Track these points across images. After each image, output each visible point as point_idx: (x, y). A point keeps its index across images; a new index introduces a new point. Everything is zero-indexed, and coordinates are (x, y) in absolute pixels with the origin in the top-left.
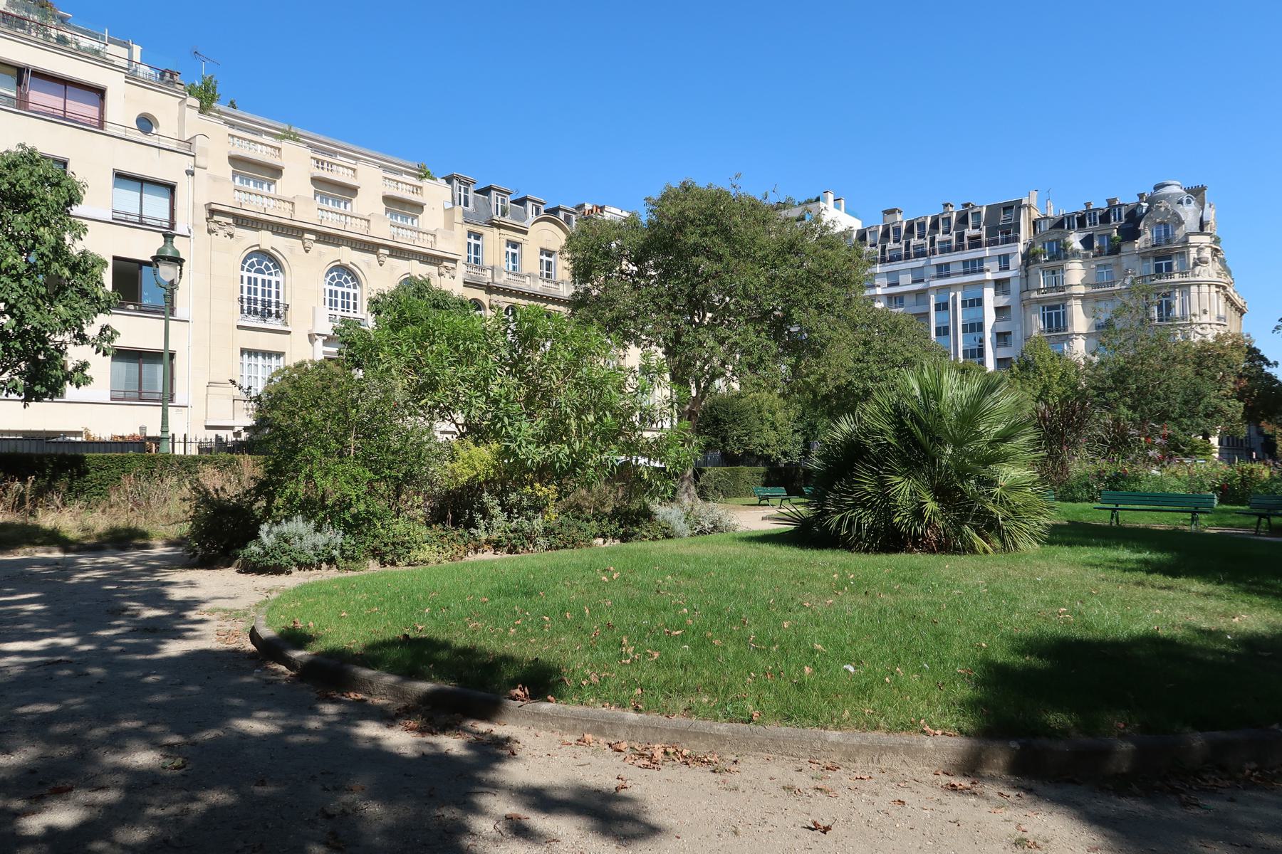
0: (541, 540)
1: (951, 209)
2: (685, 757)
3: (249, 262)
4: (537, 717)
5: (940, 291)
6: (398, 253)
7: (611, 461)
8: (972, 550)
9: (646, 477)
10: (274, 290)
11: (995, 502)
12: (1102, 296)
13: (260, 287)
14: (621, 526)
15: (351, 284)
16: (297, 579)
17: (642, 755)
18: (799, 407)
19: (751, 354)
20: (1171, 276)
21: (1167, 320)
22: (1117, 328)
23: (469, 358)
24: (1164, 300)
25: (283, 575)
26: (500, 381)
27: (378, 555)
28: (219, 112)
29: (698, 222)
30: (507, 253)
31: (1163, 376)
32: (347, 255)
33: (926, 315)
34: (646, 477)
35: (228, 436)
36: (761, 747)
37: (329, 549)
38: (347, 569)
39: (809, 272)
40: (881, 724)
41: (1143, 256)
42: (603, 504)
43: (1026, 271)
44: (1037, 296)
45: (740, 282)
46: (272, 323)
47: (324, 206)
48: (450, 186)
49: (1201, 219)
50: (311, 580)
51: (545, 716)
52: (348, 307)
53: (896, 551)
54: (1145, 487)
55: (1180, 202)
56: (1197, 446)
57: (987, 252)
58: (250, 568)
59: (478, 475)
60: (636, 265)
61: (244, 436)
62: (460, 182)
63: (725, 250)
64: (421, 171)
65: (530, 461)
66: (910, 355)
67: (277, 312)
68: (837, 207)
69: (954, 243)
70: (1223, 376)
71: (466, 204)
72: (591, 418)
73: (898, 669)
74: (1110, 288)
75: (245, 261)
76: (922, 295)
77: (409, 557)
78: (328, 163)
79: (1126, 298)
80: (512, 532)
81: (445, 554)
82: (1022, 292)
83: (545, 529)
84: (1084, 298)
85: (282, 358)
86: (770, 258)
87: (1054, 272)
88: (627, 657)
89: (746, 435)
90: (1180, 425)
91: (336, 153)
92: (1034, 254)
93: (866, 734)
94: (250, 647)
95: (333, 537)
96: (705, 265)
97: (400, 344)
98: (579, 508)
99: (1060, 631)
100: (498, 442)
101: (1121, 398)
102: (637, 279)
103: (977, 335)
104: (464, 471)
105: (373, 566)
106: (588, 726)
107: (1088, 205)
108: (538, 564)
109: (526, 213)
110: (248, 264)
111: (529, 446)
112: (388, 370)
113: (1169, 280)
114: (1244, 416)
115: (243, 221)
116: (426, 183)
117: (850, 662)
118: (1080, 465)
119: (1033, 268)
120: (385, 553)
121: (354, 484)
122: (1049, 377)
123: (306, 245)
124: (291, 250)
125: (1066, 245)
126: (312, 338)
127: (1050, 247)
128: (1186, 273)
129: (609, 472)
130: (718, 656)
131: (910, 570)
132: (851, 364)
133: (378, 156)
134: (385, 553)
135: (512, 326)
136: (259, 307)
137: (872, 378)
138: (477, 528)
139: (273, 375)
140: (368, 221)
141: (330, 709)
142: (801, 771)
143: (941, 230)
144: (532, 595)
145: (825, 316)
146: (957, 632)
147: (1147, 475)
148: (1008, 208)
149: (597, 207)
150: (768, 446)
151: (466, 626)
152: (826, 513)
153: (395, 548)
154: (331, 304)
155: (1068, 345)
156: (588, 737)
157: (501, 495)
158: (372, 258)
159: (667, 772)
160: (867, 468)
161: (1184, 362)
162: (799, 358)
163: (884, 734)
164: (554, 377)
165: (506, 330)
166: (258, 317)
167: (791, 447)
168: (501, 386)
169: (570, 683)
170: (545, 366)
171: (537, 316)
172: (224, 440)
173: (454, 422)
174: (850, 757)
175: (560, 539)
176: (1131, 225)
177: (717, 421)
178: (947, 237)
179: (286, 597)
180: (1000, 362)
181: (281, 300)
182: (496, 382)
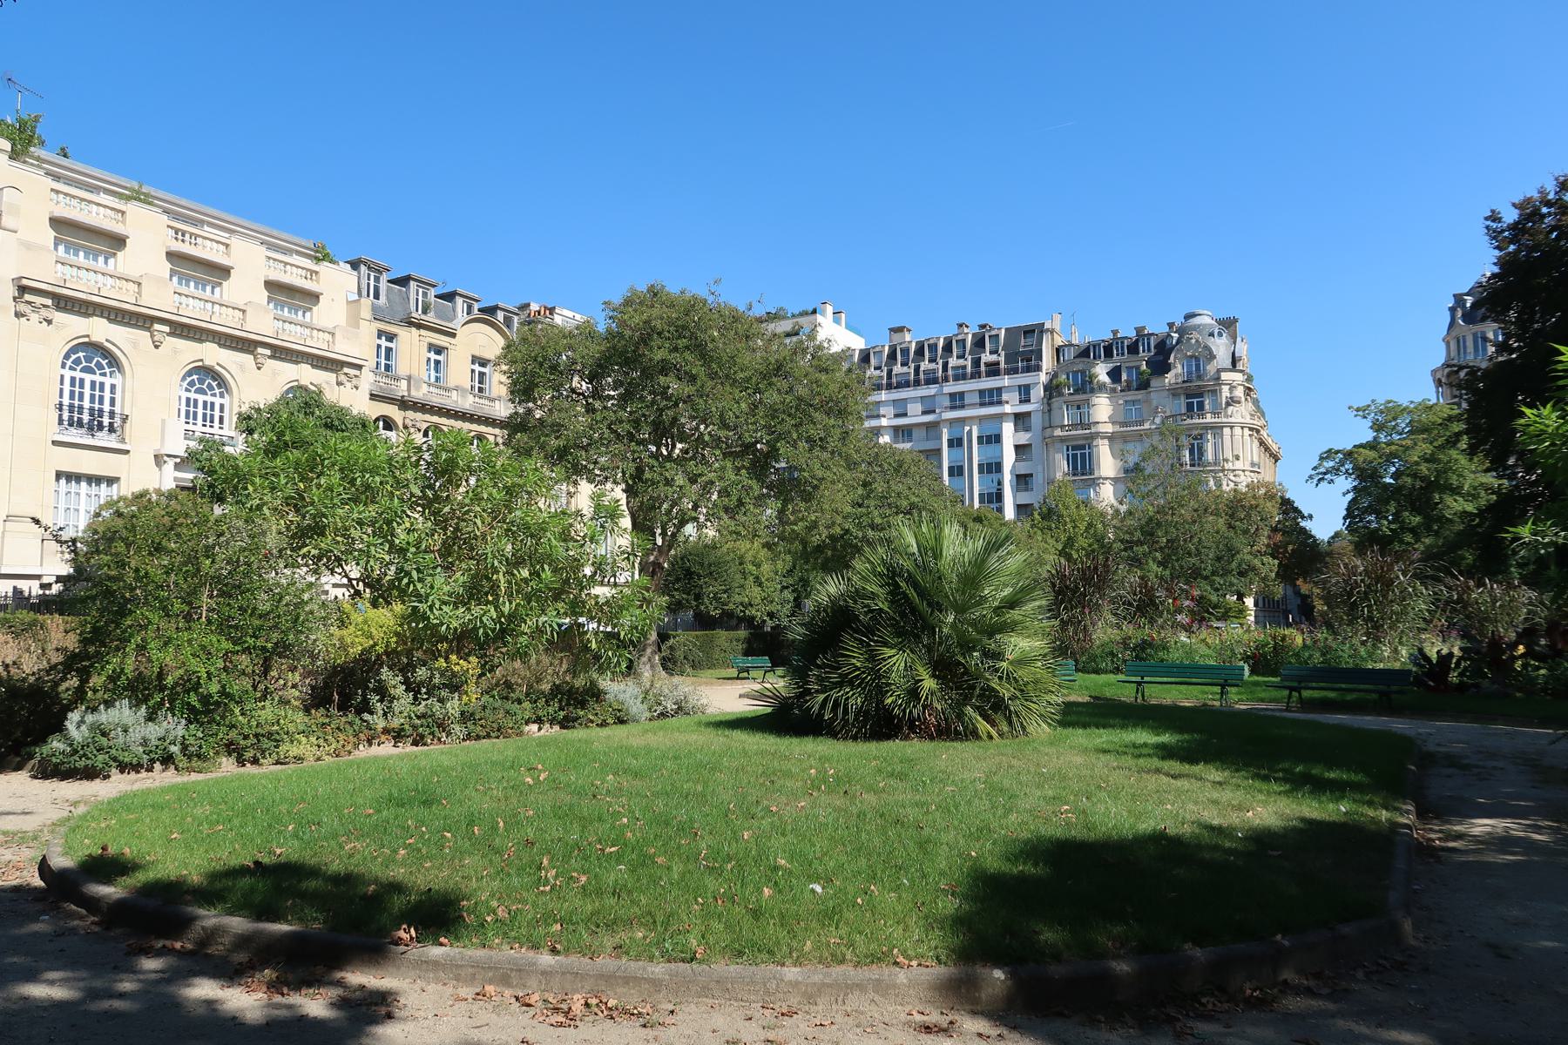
0: (457, 728)
1: (966, 330)
2: (611, 1009)
3: (74, 357)
4: (425, 965)
5: (953, 425)
6: (282, 353)
7: (550, 626)
8: (974, 734)
9: (594, 646)
10: (107, 395)
11: (1000, 678)
12: (1130, 436)
13: (87, 391)
14: (561, 709)
15: (217, 391)
16: (117, 785)
17: (556, 1010)
18: (788, 558)
19: (728, 495)
20: (1203, 416)
21: (1199, 465)
22: (1146, 473)
23: (366, 494)
24: (1196, 442)
25: (98, 781)
26: (408, 525)
27: (234, 751)
28: (38, 159)
29: (667, 335)
30: (429, 359)
31: (1196, 527)
32: (212, 354)
33: (938, 451)
34: (594, 646)
35: (32, 588)
36: (705, 991)
37: (166, 744)
38: (190, 770)
39: (798, 399)
40: (848, 957)
41: (1174, 392)
42: (539, 681)
43: (1049, 405)
44: (1061, 434)
45: (717, 408)
46: (103, 439)
47: (183, 289)
48: (355, 273)
49: (1233, 354)
50: (136, 787)
51: (435, 965)
52: (212, 421)
53: (888, 737)
54: (1175, 656)
55: (1212, 335)
56: (1230, 608)
57: (1006, 381)
58: (50, 771)
59: (375, 644)
60: (591, 383)
61: (56, 589)
62: (369, 268)
63: (698, 369)
64: (317, 252)
66: (916, 500)
67: (111, 425)
68: (837, 321)
69: (969, 369)
70: (1257, 529)
71: (377, 296)
72: (525, 573)
73: (872, 887)
74: (1139, 428)
75: (67, 356)
76: (933, 427)
77: (278, 753)
78: (191, 234)
79: (1156, 439)
80: (418, 717)
81: (327, 748)
82: (1044, 428)
83: (462, 713)
84: (1112, 438)
85: (115, 486)
86: (754, 379)
87: (1079, 408)
88: (547, 882)
89: (725, 592)
90: (1212, 584)
91: (202, 222)
92: (1057, 386)
93: (829, 970)
94: (37, 882)
95: (172, 727)
96: (675, 387)
97: (276, 475)
98: (509, 686)
99: (1059, 833)
100: (403, 602)
101: (1150, 552)
102: (591, 400)
103: (995, 476)
104: (357, 640)
105: (228, 765)
106: (490, 974)
107: (1115, 332)
108: (446, 761)
109: (454, 311)
110: (71, 360)
111: (443, 607)
112: (259, 508)
113: (1201, 421)
114: (1277, 574)
115: (65, 303)
116: (324, 268)
117: (817, 880)
118: (1105, 630)
119: (1056, 402)
120: (245, 749)
121: (204, 657)
122: (1074, 528)
123: (156, 339)
124: (135, 345)
125: (1092, 377)
126: (159, 460)
128: (1218, 413)
129: (547, 640)
130: (661, 878)
131: (901, 762)
132: (848, 509)
133: (261, 229)
134: (245, 749)
135: (427, 456)
136: (86, 418)
137: (873, 527)
138: (371, 713)
139: (101, 508)
140: (244, 311)
141: (151, 964)
142: (750, 1019)
143: (955, 354)
144: (432, 804)
145: (817, 451)
146: (944, 838)
147: (1176, 643)
148: (1029, 331)
149: (545, 308)
150: (752, 606)
151: (341, 847)
152: (808, 692)
153: (259, 741)
154: (187, 416)
155: (1095, 490)
156: (490, 989)
157: (406, 670)
158: (247, 359)
159: (586, 1030)
160: (856, 639)
161: (1216, 513)
162: (785, 502)
163: (850, 969)
164: (479, 522)
165: (418, 461)
166: (83, 431)
167: (779, 607)
168: (409, 531)
169: (470, 919)
170: (467, 508)
171: (458, 445)
172: (26, 594)
173: (346, 576)
174: (811, 999)
175: (482, 726)
177: (689, 574)
178: (961, 362)
179: (96, 813)
180: (1021, 509)
181: (117, 409)
182: (403, 527)
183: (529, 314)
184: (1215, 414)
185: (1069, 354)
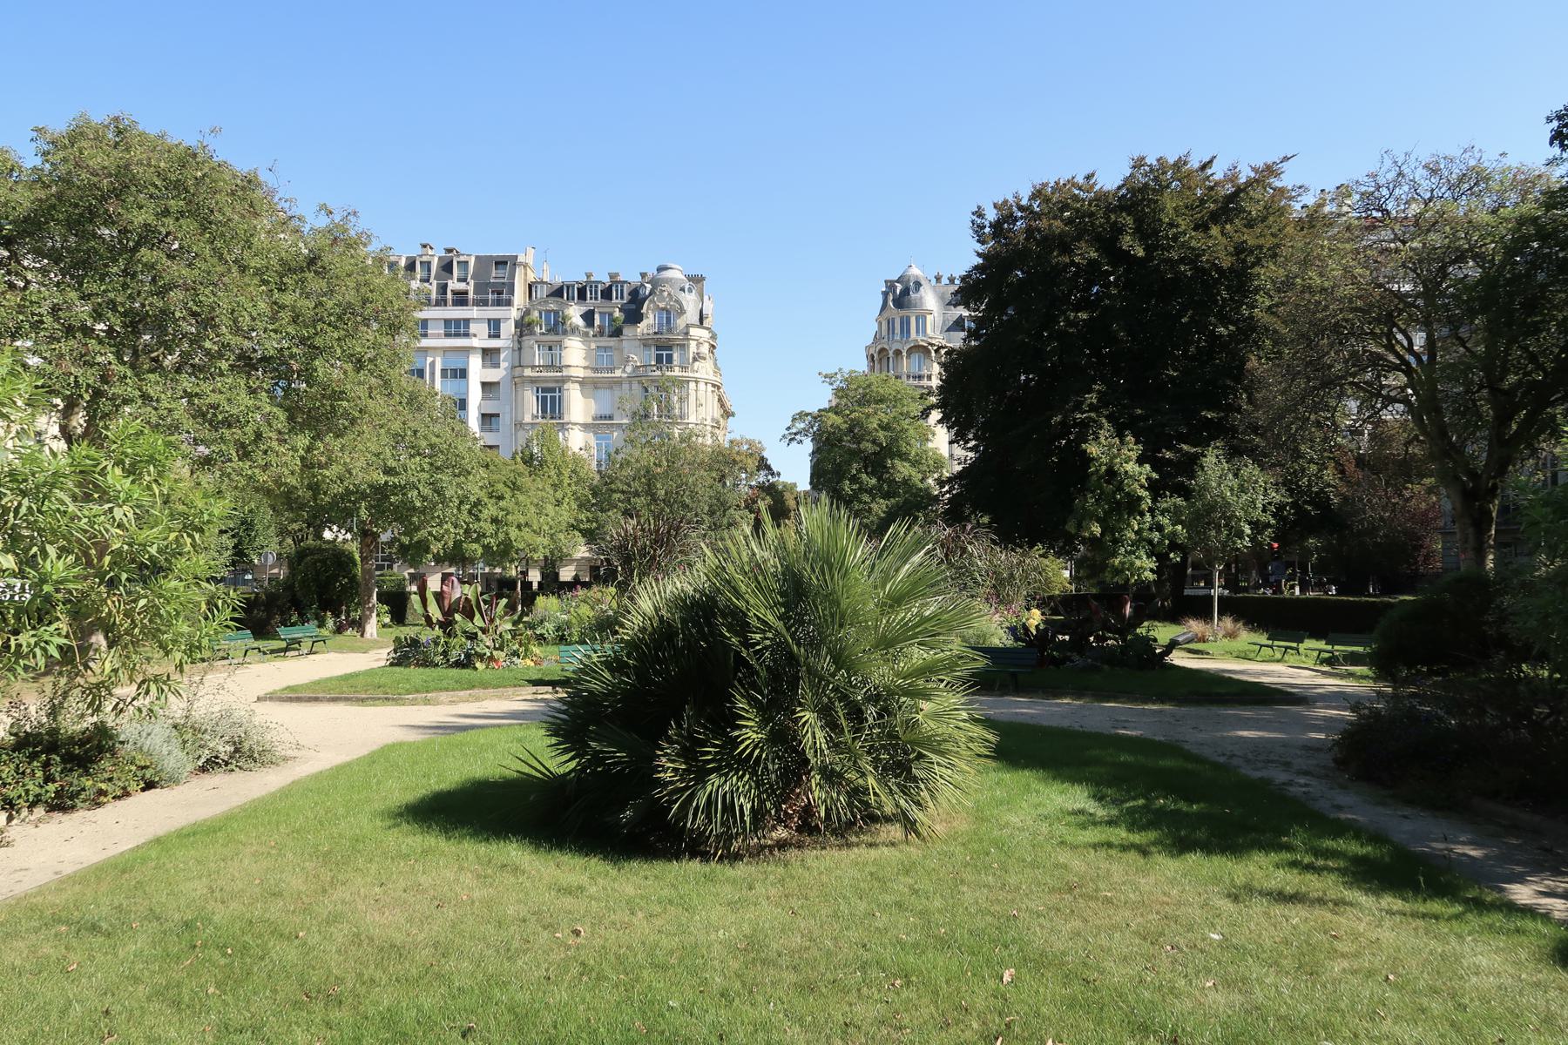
1: (430, 252)
14: (48, 779)
41: (645, 343)
43: (519, 342)
44: (531, 374)
55: (682, 290)
63: (202, 246)
69: (434, 296)
74: (610, 375)
84: (583, 383)
119: (529, 341)
127: (548, 319)
148: (501, 263)
155: (564, 434)
176: (633, 307)
184: (683, 368)
185: (542, 292)
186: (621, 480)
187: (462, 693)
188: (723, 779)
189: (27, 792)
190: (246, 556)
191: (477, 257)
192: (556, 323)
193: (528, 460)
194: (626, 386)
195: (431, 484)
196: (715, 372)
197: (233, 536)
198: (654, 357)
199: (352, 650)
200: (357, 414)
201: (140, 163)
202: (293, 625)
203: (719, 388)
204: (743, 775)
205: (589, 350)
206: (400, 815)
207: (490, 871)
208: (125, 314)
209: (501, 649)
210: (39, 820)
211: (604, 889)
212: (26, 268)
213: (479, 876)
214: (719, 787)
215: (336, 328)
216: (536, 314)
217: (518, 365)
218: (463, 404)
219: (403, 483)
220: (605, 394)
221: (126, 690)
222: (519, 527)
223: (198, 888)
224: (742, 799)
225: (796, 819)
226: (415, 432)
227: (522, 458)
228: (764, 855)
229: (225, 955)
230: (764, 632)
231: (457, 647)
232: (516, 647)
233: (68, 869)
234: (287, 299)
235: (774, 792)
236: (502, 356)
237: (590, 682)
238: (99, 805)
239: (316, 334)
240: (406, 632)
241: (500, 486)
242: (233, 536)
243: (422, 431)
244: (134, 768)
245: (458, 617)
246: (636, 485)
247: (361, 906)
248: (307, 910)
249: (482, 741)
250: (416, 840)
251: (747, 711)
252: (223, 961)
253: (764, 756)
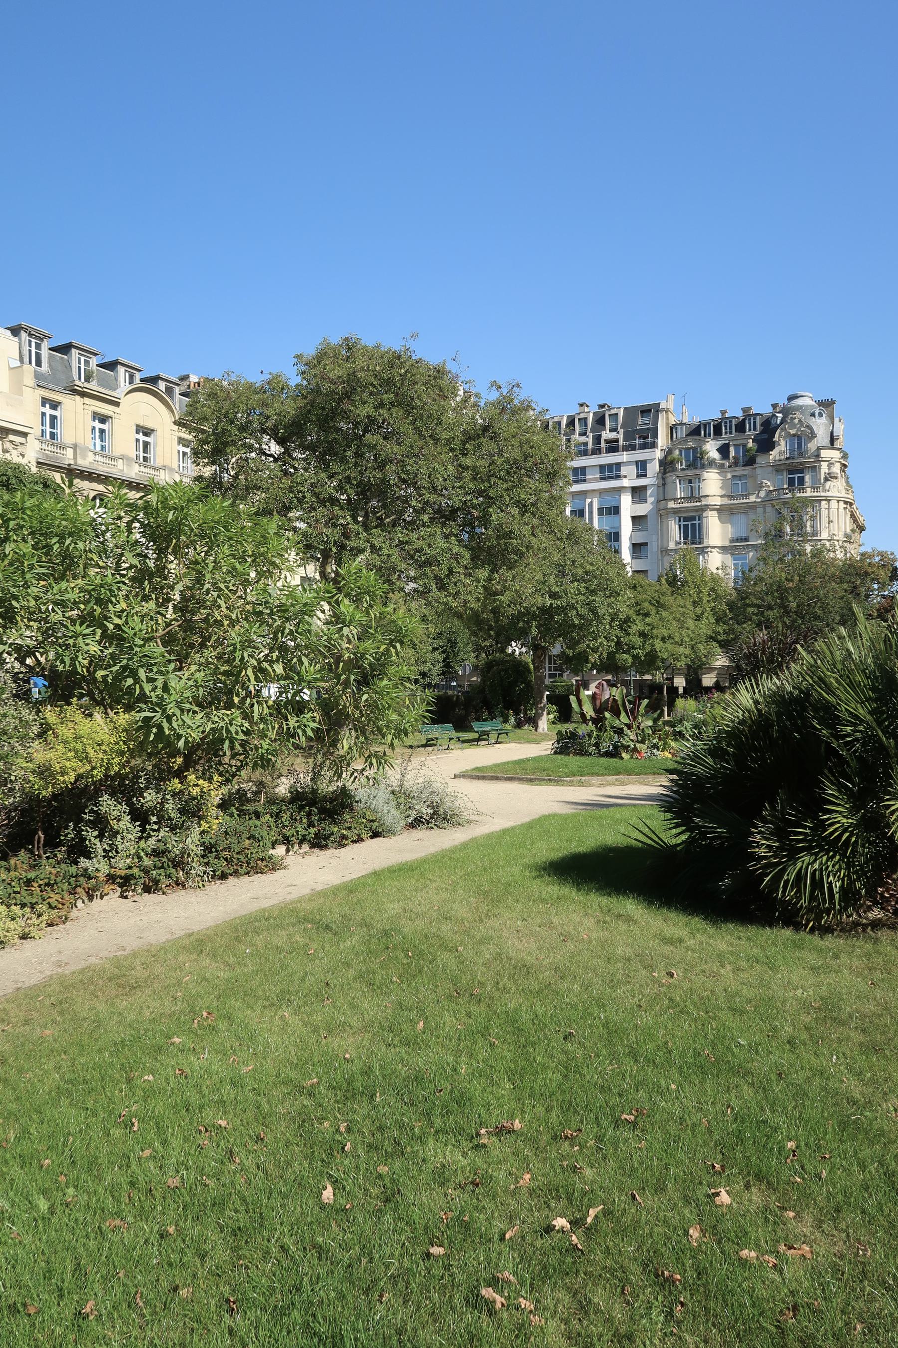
1: (586, 410)
14: (311, 825)
30: (94, 428)
41: (778, 468)
43: (663, 479)
44: (674, 506)
48: (16, 339)
49: (832, 433)
55: (813, 415)
57: (624, 457)
62: (30, 335)
63: (406, 428)
65: (183, 740)
69: (590, 446)
71: (39, 364)
74: (745, 501)
84: (720, 510)
87: (690, 482)
107: (723, 413)
109: (116, 380)
113: (802, 495)
119: (672, 477)
125: (703, 453)
127: (687, 456)
148: (645, 411)
155: (704, 557)
175: (226, 859)
176: (766, 436)
178: (583, 439)
183: (189, 386)
184: (815, 488)
185: (682, 433)
186: (755, 595)
187: (610, 778)
188: (813, 858)
189: (297, 832)
190: (452, 667)
191: (625, 409)
192: (695, 458)
193: (673, 581)
194: (760, 510)
195: (587, 604)
196: (847, 490)
197: (443, 652)
198: (786, 480)
199: (529, 741)
200: (524, 550)
201: (362, 369)
202: (485, 720)
203: (851, 504)
204: (834, 856)
205: (725, 481)
206: (545, 869)
207: (608, 918)
208: (357, 486)
209: (642, 742)
210: (306, 853)
211: (701, 943)
212: (294, 459)
213: (599, 921)
214: (808, 864)
215: (506, 480)
216: (677, 452)
217: (662, 499)
218: (615, 536)
219: (564, 604)
220: (741, 519)
221: (358, 765)
222: (663, 639)
223: (394, 908)
224: (831, 878)
225: (893, 903)
226: (574, 562)
227: (666, 580)
228: (856, 931)
229: (407, 956)
230: (854, 725)
231: (607, 740)
232: (655, 741)
233: (319, 887)
234: (468, 461)
235: (865, 873)
236: (649, 492)
237: (696, 767)
238: (343, 846)
239: (490, 487)
240: (570, 727)
241: (646, 604)
242: (443, 652)
243: (579, 560)
244: (364, 821)
245: (607, 715)
246: (769, 598)
247: (506, 933)
248: (467, 933)
249: (618, 816)
250: (552, 888)
251: (837, 798)
252: (405, 961)
253: (853, 839)
